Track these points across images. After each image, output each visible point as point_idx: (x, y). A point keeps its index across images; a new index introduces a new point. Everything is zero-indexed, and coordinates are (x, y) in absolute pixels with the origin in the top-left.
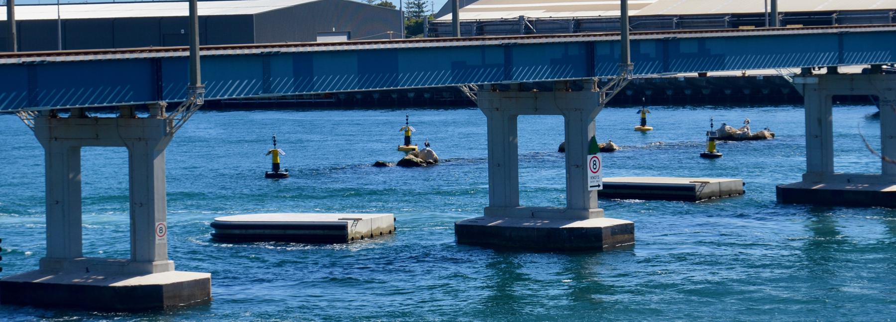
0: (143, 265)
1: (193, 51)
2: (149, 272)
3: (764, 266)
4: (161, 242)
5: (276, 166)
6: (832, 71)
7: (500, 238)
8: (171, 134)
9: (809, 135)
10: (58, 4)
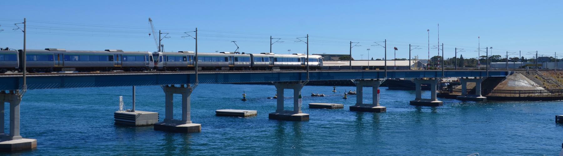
0: (184, 122)
1: (23, 74)
2: (185, 123)
3: (446, 114)
4: (189, 116)
6: (467, 78)
7: (359, 110)
10: (385, 60)
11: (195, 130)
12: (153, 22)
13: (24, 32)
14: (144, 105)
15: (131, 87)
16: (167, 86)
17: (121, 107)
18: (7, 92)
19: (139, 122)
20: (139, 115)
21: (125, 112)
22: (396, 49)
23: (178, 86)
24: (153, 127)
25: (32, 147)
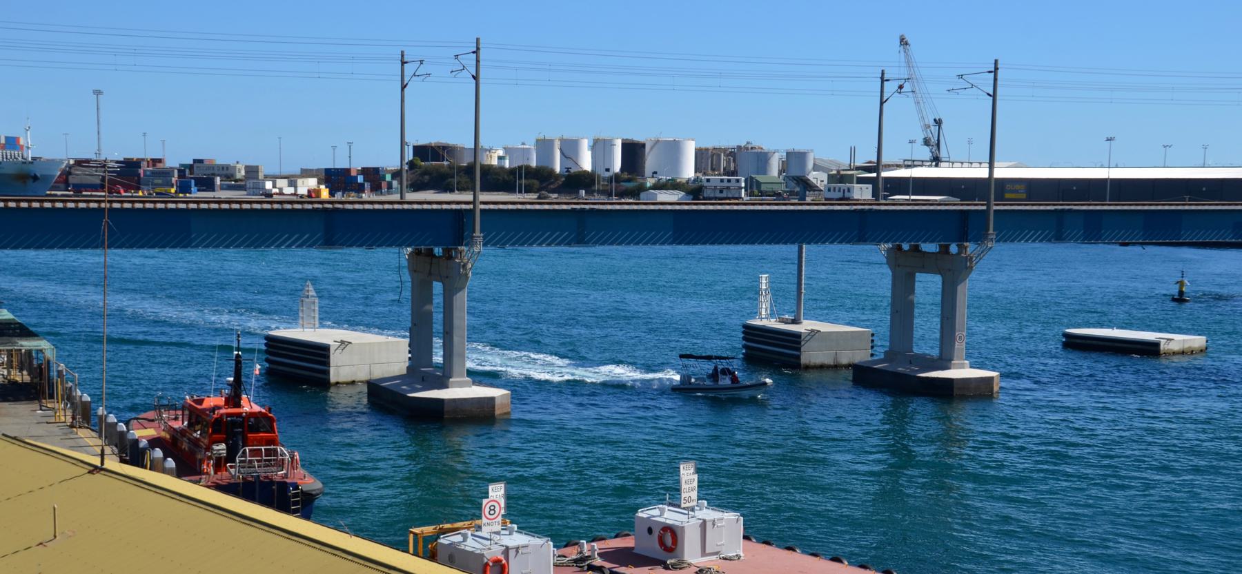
0: (944, 363)
1: (988, 205)
2: (948, 368)
4: (960, 346)
5: (1181, 293)
8: (971, 268)
9: (911, 316)
11: (980, 392)
12: (914, 48)
13: (476, 78)
14: (828, 308)
15: (795, 248)
16: (899, 248)
17: (765, 306)
18: (438, 251)
19: (811, 355)
20: (813, 333)
21: (773, 324)
22: (98, 93)
23: (930, 247)
24: (849, 374)
25: (497, 412)
